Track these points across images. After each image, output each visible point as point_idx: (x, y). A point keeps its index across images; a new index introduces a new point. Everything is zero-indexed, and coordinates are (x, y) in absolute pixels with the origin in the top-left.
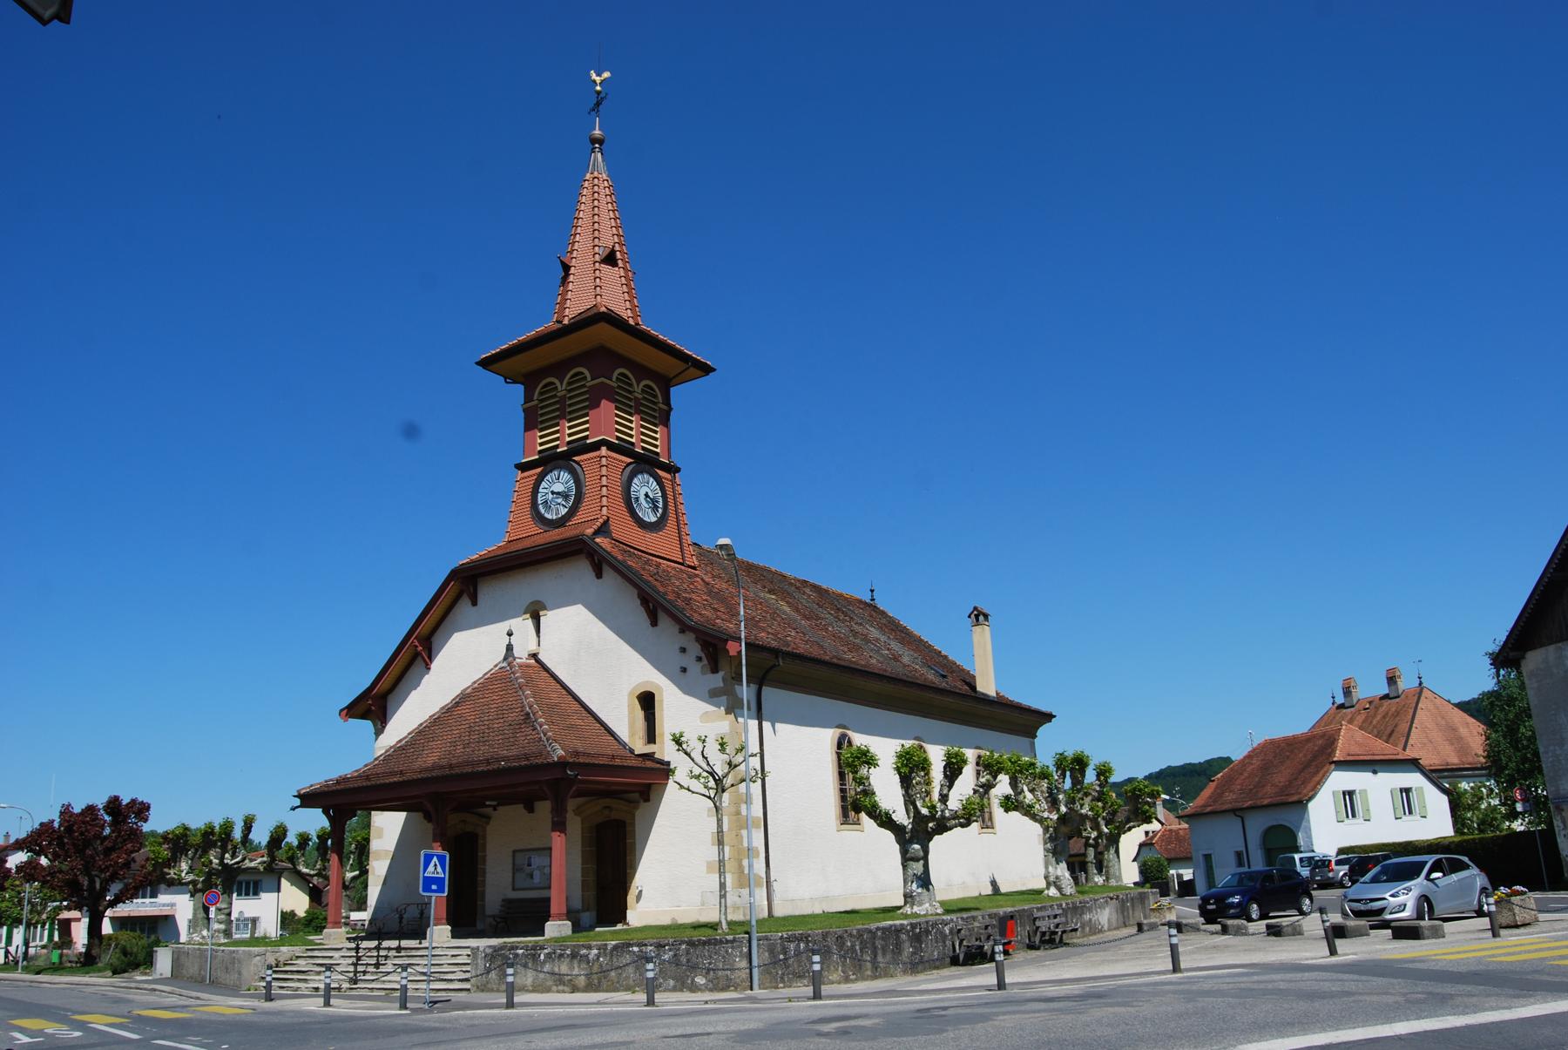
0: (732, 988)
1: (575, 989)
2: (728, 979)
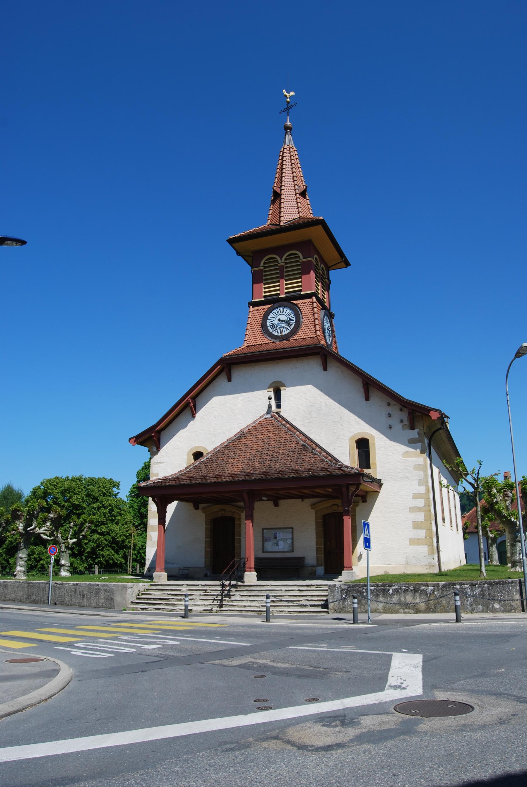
0: (513, 611)
1: (417, 611)
2: (511, 605)
